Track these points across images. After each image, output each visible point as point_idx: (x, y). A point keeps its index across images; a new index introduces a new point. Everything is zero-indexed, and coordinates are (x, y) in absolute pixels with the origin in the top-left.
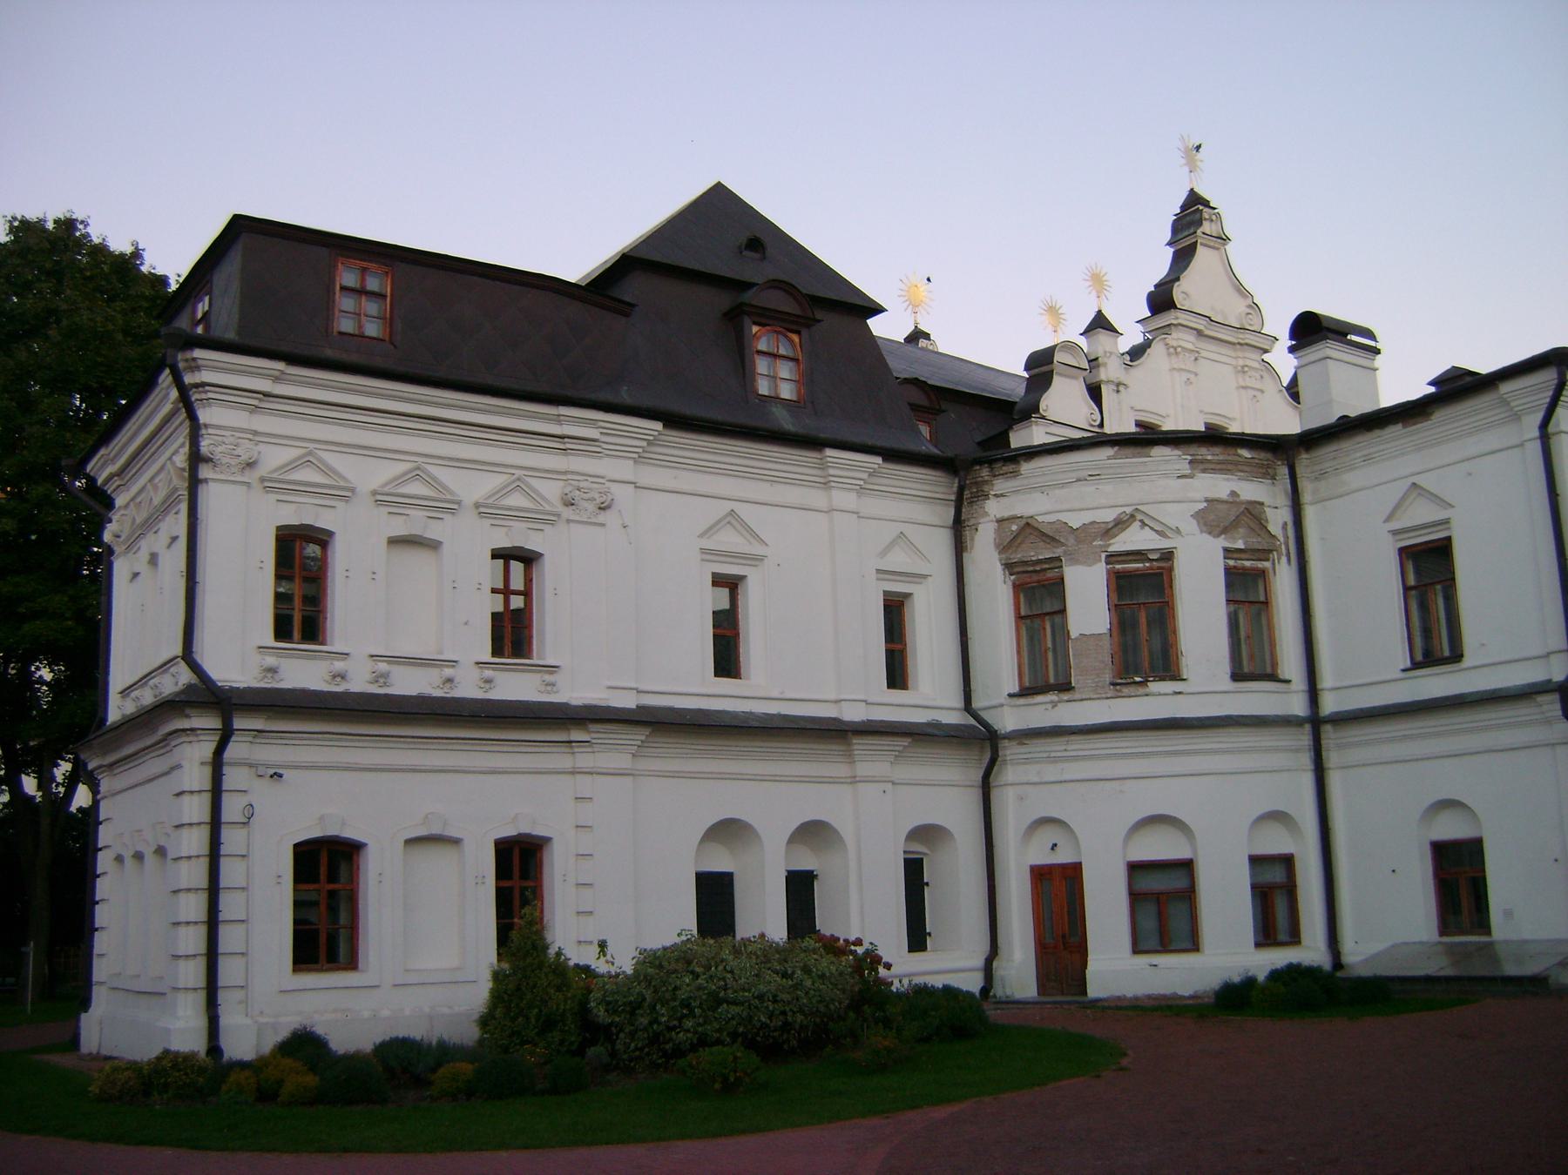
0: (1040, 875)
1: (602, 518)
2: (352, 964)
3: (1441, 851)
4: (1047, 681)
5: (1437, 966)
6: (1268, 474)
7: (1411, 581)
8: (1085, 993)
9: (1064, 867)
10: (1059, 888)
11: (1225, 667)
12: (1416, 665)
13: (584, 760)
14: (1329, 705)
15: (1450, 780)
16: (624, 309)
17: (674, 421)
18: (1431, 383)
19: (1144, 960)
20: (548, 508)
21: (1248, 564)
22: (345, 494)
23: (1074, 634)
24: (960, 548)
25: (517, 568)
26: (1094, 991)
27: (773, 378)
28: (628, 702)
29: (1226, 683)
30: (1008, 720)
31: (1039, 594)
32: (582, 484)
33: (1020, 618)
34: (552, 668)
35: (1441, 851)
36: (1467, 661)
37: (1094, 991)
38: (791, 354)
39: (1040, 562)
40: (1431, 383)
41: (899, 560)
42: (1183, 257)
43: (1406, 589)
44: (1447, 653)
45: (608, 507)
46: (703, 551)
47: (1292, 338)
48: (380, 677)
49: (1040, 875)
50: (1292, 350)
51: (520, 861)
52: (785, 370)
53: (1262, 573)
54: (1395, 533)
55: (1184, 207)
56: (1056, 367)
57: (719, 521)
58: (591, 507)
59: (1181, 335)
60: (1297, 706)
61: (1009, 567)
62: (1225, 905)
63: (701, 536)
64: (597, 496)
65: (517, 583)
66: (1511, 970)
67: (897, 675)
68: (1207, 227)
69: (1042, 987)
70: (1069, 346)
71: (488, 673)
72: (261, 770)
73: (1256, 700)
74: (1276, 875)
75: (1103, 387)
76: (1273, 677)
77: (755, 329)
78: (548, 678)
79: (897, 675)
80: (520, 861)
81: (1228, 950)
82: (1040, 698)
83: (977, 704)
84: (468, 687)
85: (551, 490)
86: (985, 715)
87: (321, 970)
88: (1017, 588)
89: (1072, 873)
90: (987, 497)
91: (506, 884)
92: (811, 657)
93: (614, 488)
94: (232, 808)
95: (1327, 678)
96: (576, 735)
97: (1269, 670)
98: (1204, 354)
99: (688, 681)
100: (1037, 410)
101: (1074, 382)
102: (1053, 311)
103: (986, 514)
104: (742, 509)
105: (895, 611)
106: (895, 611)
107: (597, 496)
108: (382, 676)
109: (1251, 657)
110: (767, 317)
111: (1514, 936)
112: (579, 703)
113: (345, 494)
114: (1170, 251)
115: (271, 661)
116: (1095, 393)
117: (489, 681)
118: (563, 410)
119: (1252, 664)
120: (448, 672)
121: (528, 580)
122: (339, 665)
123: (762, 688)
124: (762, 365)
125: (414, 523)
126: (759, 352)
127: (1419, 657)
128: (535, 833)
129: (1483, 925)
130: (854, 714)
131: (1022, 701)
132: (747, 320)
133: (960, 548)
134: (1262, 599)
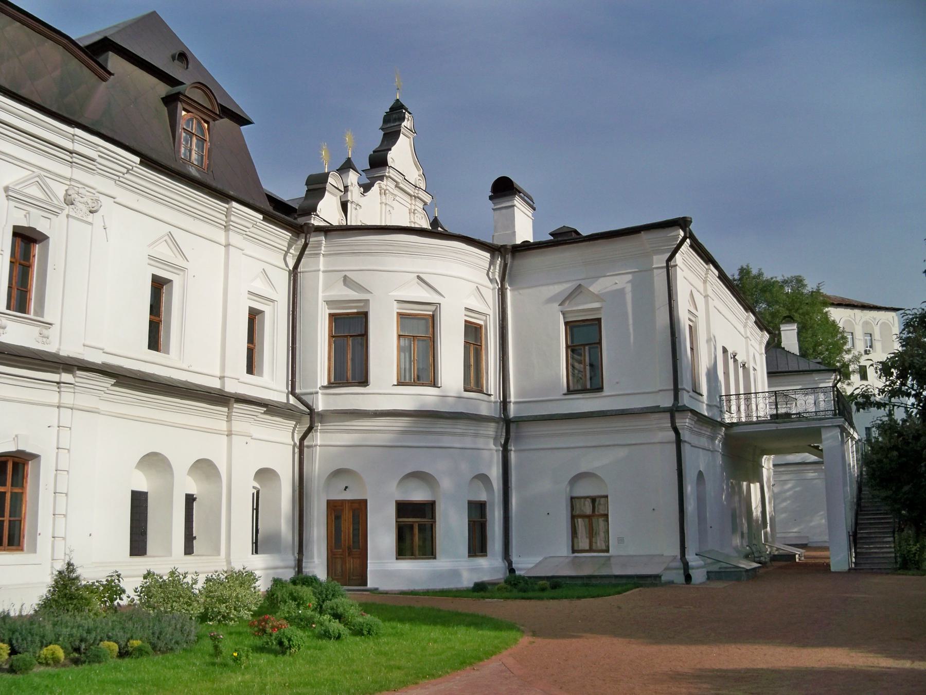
0: (404, 509)
1: (90, 218)
3: (471, 504)
5: (567, 572)
9: (352, 502)
13: (68, 397)
15: (591, 462)
16: (104, 73)
17: (148, 162)
18: (551, 234)
20: (56, 202)
30: (321, 404)
32: (81, 191)
33: (331, 336)
35: (471, 504)
36: (607, 391)
40: (551, 234)
41: (260, 287)
44: (589, 387)
46: (151, 257)
49: (335, 508)
50: (491, 198)
55: (392, 109)
56: (328, 187)
58: (85, 209)
59: (389, 183)
64: (89, 201)
75: (349, 204)
81: (453, 565)
85: (60, 190)
92: (203, 348)
93: (102, 198)
96: (66, 377)
98: (397, 198)
100: (315, 210)
101: (335, 198)
104: (177, 233)
107: (89, 201)
110: (192, 105)
116: (344, 206)
118: (78, 131)
123: (185, 360)
132: (180, 106)
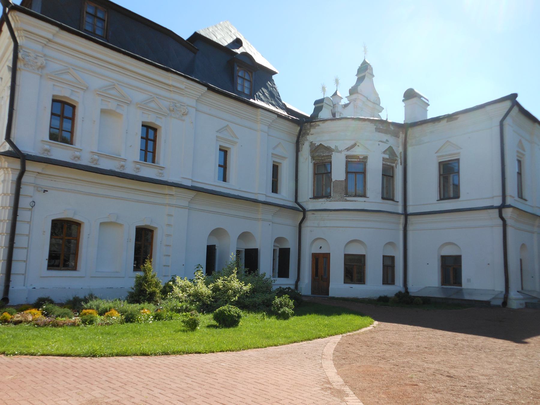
2: (74, 268)
3: (444, 259)
4: (323, 194)
6: (397, 136)
7: (442, 173)
8: (328, 295)
10: (321, 262)
11: (380, 196)
12: (441, 199)
14: (410, 210)
19: (348, 286)
21: (388, 163)
22: (86, 89)
23: (333, 180)
24: (298, 150)
25: (151, 132)
26: (332, 294)
27: (243, 86)
28: (189, 184)
29: (379, 199)
30: (311, 205)
31: (322, 169)
34: (162, 168)
35: (444, 259)
36: (461, 199)
37: (332, 294)
38: (248, 79)
39: (324, 156)
42: (360, 80)
43: (440, 175)
45: (186, 114)
47: (404, 97)
48: (93, 160)
51: (144, 238)
52: (247, 84)
53: (393, 167)
54: (438, 157)
57: (223, 128)
60: (400, 210)
61: (313, 158)
62: (374, 270)
63: (217, 132)
65: (151, 136)
66: (467, 297)
67: (275, 189)
68: (368, 71)
69: (313, 292)
70: (328, 98)
71: (138, 166)
72: (40, 189)
73: (387, 206)
74: (389, 263)
76: (393, 200)
77: (238, 68)
78: (160, 171)
79: (275, 189)
80: (144, 238)
82: (320, 200)
83: (300, 200)
84: (130, 170)
86: (302, 204)
87: (61, 270)
88: (315, 164)
89: (327, 256)
90: (308, 134)
91: (59, 139)
94: (24, 202)
95: (410, 202)
97: (392, 198)
99: (209, 177)
102: (324, 89)
103: (307, 140)
105: (276, 168)
106: (276, 168)
108: (95, 160)
109: (387, 193)
111: (470, 287)
112: (171, 181)
113: (86, 89)
114: (356, 78)
115: (47, 147)
117: (138, 169)
119: (387, 195)
120: (122, 163)
121: (155, 136)
122: (77, 154)
123: (235, 184)
124: (239, 81)
125: (111, 105)
126: (239, 76)
127: (442, 197)
128: (151, 225)
129: (460, 284)
130: (262, 198)
131: (314, 200)
133: (298, 150)
134: (391, 175)
